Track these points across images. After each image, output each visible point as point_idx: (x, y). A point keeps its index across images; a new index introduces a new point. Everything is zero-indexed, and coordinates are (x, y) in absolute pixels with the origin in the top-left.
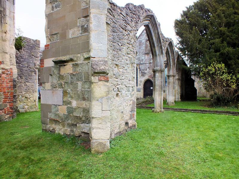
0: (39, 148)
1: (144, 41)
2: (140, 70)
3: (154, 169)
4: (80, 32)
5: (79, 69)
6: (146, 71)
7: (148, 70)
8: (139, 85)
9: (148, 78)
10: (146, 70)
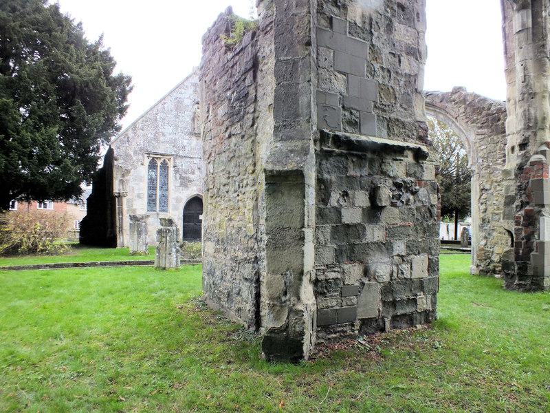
0: (7, 109)
1: (188, 102)
2: (177, 172)
3: (48, 289)
6: (191, 177)
8: (173, 210)
9: (196, 193)
10: (193, 173)
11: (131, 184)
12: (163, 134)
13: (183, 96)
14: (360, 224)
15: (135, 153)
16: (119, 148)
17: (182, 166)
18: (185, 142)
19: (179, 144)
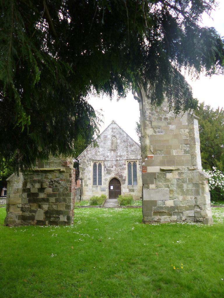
2: (105, 167)
4: (183, 153)
5: (184, 176)
7: (114, 167)
9: (114, 176)
10: (112, 167)
11: (86, 174)
12: (99, 152)
13: (107, 134)
14: (37, 193)
15: (87, 161)
16: (81, 160)
17: (107, 164)
18: (109, 154)
19: (106, 155)
